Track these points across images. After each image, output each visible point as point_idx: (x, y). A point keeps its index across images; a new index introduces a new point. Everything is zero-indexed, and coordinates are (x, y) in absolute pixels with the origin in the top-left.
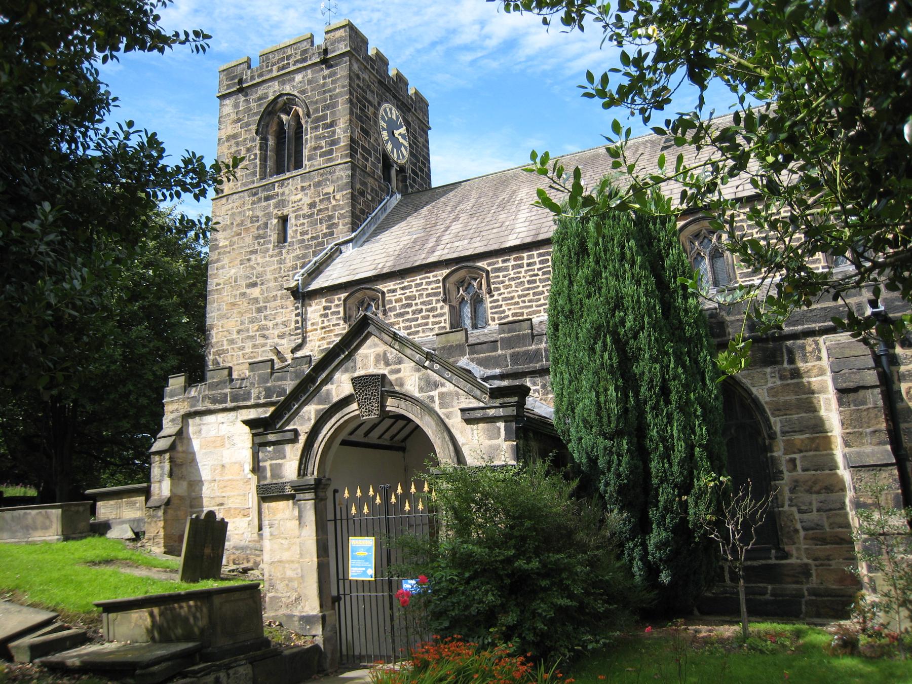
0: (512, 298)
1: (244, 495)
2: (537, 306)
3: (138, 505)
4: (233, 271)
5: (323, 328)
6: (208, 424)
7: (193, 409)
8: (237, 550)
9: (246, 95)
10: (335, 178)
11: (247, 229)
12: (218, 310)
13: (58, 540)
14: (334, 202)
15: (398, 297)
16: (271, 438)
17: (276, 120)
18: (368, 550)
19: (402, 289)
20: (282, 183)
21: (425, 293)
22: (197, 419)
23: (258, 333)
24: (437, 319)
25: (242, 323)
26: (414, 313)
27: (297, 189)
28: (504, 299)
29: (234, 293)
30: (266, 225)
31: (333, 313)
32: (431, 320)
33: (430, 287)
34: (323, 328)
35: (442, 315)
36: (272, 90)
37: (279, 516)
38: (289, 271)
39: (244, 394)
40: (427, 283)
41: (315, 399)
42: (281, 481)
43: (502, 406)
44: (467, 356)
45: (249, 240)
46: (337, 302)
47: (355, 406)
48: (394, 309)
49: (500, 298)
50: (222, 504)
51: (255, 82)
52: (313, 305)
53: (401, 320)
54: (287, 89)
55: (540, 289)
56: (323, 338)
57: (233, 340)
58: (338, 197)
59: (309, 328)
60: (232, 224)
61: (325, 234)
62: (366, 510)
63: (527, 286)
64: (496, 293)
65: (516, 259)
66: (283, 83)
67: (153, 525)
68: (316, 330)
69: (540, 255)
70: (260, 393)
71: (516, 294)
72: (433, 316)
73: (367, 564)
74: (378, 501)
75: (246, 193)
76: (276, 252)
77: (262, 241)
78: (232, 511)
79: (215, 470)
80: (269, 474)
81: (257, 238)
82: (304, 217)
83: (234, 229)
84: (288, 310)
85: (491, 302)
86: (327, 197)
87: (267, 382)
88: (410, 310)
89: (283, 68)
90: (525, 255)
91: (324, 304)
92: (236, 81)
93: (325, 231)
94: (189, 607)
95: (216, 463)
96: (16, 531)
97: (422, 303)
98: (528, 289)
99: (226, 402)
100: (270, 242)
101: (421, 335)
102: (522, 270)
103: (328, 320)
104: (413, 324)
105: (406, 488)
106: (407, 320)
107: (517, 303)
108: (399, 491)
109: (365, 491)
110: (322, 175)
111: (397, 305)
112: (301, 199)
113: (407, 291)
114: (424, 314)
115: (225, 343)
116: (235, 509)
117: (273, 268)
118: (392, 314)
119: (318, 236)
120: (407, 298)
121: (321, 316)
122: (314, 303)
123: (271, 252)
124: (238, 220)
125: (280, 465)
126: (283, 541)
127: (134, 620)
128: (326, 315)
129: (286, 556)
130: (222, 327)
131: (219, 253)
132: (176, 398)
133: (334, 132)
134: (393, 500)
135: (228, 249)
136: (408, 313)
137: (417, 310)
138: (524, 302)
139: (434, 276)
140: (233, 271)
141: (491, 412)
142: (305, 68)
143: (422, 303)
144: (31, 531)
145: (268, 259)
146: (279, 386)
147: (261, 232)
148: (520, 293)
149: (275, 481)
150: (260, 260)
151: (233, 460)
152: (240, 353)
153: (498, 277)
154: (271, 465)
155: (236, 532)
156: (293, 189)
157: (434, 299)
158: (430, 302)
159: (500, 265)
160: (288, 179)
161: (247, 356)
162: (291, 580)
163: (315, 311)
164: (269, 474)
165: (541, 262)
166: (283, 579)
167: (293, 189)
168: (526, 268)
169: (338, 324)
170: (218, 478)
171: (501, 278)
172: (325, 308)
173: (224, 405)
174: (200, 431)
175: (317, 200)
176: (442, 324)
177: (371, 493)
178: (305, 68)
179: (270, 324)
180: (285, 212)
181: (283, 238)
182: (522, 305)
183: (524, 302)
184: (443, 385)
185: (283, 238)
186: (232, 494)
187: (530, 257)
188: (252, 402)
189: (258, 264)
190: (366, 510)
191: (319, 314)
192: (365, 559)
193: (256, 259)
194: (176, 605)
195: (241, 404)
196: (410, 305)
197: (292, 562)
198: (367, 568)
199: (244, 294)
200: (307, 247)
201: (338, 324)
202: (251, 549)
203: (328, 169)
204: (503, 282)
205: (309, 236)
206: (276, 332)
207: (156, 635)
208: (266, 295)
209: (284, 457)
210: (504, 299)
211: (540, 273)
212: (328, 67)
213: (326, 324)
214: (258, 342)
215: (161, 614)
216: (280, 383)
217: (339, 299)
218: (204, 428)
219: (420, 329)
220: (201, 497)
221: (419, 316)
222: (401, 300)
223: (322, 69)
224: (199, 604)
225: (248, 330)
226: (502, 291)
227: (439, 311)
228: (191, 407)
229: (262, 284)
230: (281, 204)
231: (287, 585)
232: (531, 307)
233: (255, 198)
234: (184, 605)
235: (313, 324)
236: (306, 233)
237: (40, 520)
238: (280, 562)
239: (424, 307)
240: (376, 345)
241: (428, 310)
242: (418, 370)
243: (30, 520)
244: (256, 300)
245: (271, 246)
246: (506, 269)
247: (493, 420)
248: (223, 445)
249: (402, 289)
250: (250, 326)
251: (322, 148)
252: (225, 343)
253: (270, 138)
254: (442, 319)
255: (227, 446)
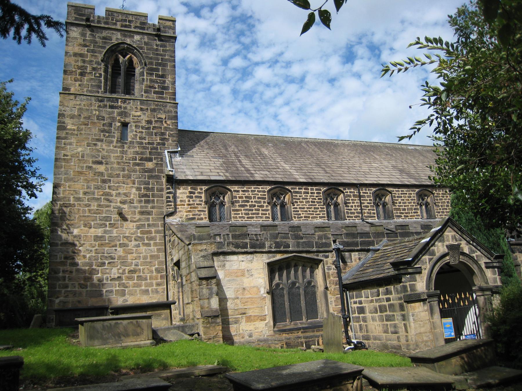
0: (304, 208)
1: (262, 307)
2: (316, 214)
3: (163, 316)
4: (80, 149)
5: (189, 205)
6: (231, 261)
7: (220, 250)
8: (261, 342)
9: (92, 31)
10: (166, 110)
11: (94, 123)
12: (65, 174)
13: (151, 343)
14: (165, 125)
15: (240, 195)
16: (410, 270)
17: (114, 56)
18: (450, 324)
19: (243, 191)
20: (124, 101)
21: (257, 196)
22: (221, 257)
23: (103, 197)
24: (264, 212)
25: (88, 187)
26: (250, 206)
27: (136, 108)
28: (300, 208)
29: (81, 165)
30: (110, 125)
31: (196, 197)
32: (260, 212)
33: (260, 194)
34: (189, 205)
35: (267, 210)
36: (116, 38)
37: (417, 310)
38: (130, 160)
39: (260, 244)
40: (258, 191)
41: (428, 253)
42: (416, 293)
43: (498, 262)
44: (386, 238)
45: (95, 130)
46: (199, 190)
47: (448, 258)
48: (238, 202)
49: (298, 207)
50: (244, 314)
51: (99, 25)
52: (181, 188)
53: (243, 209)
54: (128, 41)
55: (317, 206)
56: (190, 211)
57: (80, 198)
58: (168, 122)
59: (178, 203)
60: (80, 115)
61: (159, 143)
62: (446, 306)
63: (311, 203)
64: (296, 204)
65: (305, 189)
66: (125, 36)
67: (211, 328)
68: (184, 205)
69: (316, 190)
70: (271, 244)
71: (306, 207)
72: (262, 210)
73: (451, 330)
74: (450, 301)
75: (93, 98)
76: (119, 144)
77: (107, 134)
78: (252, 318)
79: (238, 291)
80: (409, 289)
81: (102, 131)
82: (143, 128)
83: (82, 120)
84: (129, 186)
85: (293, 208)
86: (160, 120)
87: (277, 238)
88: (248, 204)
89: (126, 26)
90: (309, 188)
91: (190, 190)
92: (84, 18)
93: (159, 141)
94: (482, 350)
95: (238, 287)
96: (108, 339)
97: (255, 202)
98: (311, 205)
99: (247, 248)
100: (114, 137)
101: (255, 219)
102: (309, 195)
103: (193, 201)
104: (250, 212)
105: (460, 295)
106: (246, 210)
107: (306, 211)
108: (458, 297)
109: (465, 295)
110: (157, 105)
111: (240, 200)
112: (140, 116)
113: (247, 193)
114: (256, 208)
115: (72, 199)
116: (255, 316)
117: (116, 155)
118: (237, 204)
119: (154, 143)
120: (246, 197)
121: (188, 197)
122: (181, 188)
123: (115, 144)
124: (85, 114)
125: (414, 284)
126: (420, 323)
127: (453, 363)
128: (191, 197)
129: (423, 330)
130: (69, 187)
131: (67, 133)
132: (204, 241)
133: (164, 82)
134: (456, 301)
135: (76, 132)
136: (247, 206)
137: (252, 205)
138: (310, 211)
139: (262, 188)
140: (80, 149)
141: (495, 264)
142: (143, 34)
143: (255, 202)
144: (123, 338)
145: (112, 148)
146: (285, 242)
147: (106, 128)
148: (308, 206)
149: (413, 293)
150: (104, 147)
151: (252, 285)
152: (87, 209)
153: (297, 196)
154: (409, 285)
155: (257, 331)
156: (134, 107)
157: (262, 201)
158: (260, 202)
159: (297, 190)
160: (130, 99)
161: (92, 212)
162: (427, 341)
163: (184, 193)
164: (409, 289)
165: (317, 193)
166: (423, 342)
167: (134, 107)
168: (310, 194)
169: (201, 204)
170: (240, 297)
171: (298, 197)
172: (191, 193)
173: (246, 250)
174: (224, 265)
175: (153, 120)
176: (267, 215)
177: (447, 298)
178: (143, 34)
179: (114, 193)
180: (127, 120)
181: (123, 138)
182: (309, 212)
183: (310, 211)
184: (476, 252)
185: (123, 138)
186: (252, 306)
187: (312, 189)
188: (266, 249)
189: (103, 149)
190: (446, 306)
191: (186, 195)
192: (450, 328)
193: (102, 146)
194: (475, 351)
195: (258, 250)
196: (248, 202)
197: (426, 332)
198: (451, 332)
199: (90, 168)
200: (144, 148)
201: (201, 204)
202: (271, 340)
203: (161, 103)
204: (299, 199)
205: (147, 141)
206: (119, 199)
207: (466, 367)
208: (110, 172)
209: (416, 281)
210: (300, 208)
211: (317, 198)
212: (160, 40)
213: (191, 202)
214: (102, 203)
215: (468, 357)
216: (285, 240)
217: (201, 189)
218: (228, 264)
219: (254, 216)
220: (227, 309)
221: (254, 208)
222: (242, 197)
223: (156, 40)
224: (486, 348)
225: (94, 193)
226: (299, 203)
227: (265, 208)
228: (218, 248)
229: (107, 164)
230: (124, 114)
231: (425, 344)
232: (313, 214)
233: (101, 104)
234: (479, 350)
235: (181, 201)
236: (144, 138)
237: (131, 328)
238: (420, 333)
239: (256, 204)
240: (450, 232)
241: (258, 206)
242: (467, 245)
243: (121, 329)
244: (101, 174)
245: (115, 140)
246: (301, 193)
247: (493, 267)
248: (243, 275)
249: (243, 191)
250: (96, 191)
251: (156, 88)
252: (72, 199)
253: (110, 67)
254: (267, 212)
255: (247, 276)
